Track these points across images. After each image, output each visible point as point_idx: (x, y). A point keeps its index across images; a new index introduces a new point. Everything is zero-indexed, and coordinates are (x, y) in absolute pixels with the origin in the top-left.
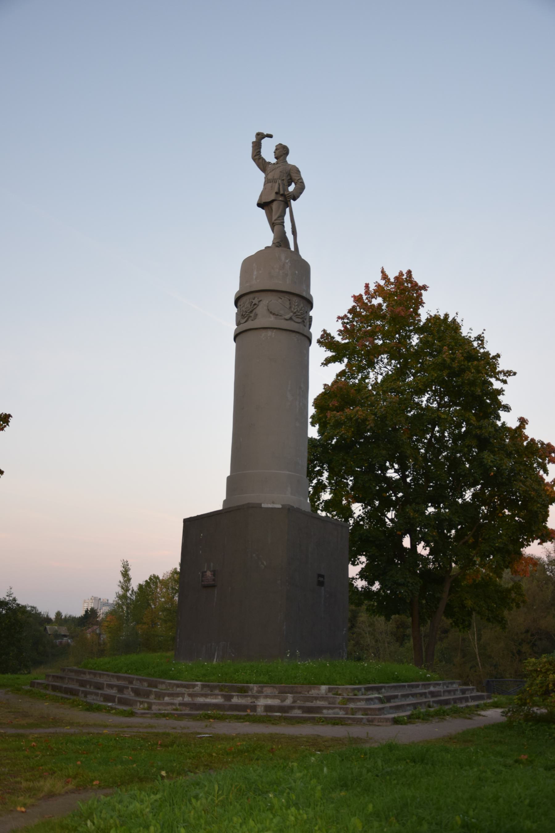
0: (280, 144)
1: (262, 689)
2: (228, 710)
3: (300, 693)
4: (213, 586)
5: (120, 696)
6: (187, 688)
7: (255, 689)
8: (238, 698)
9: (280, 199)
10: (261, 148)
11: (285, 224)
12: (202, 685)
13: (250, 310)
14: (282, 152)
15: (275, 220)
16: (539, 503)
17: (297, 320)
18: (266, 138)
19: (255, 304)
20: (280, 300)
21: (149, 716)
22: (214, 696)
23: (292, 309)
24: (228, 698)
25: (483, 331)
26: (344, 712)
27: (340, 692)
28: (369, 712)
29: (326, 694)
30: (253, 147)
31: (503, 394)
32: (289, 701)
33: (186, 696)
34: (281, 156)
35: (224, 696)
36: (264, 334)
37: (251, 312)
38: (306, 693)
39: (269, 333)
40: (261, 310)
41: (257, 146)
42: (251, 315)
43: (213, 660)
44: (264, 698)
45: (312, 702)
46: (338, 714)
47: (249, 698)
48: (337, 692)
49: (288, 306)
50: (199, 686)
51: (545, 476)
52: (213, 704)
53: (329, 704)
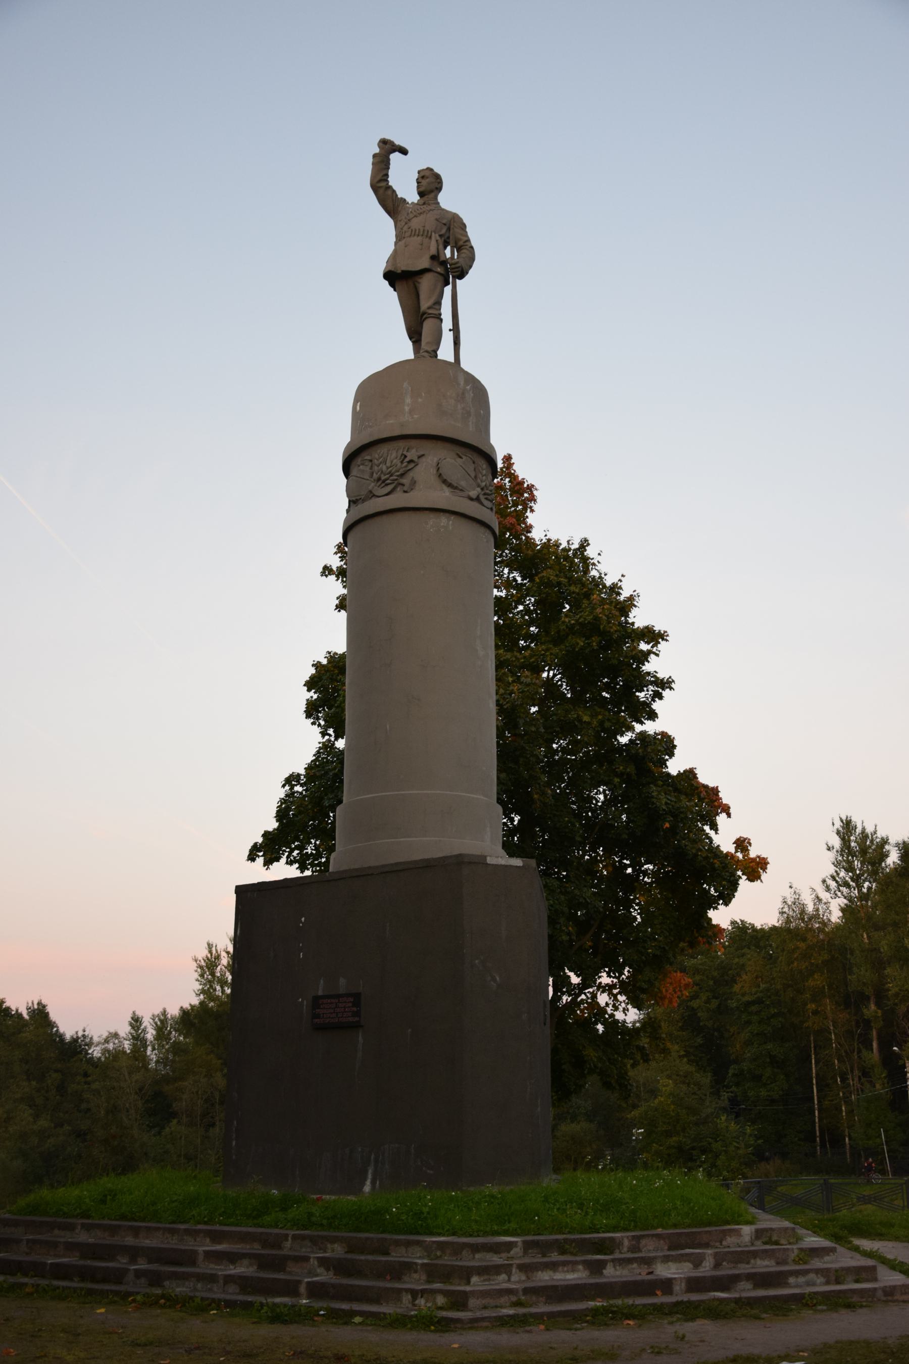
0: (430, 170)
3: (777, 1243)
4: (356, 1026)
5: (309, 1280)
7: (626, 1243)
8: (614, 1267)
9: (439, 270)
10: (389, 168)
12: (524, 1242)
13: (401, 471)
14: (430, 184)
15: (429, 308)
16: (725, 879)
18: (397, 153)
19: (411, 461)
20: (459, 460)
21: (485, 1324)
22: (570, 1267)
24: (596, 1268)
26: (822, 1280)
29: (752, 1244)
31: (671, 688)
32: (708, 1264)
33: (514, 1270)
34: (432, 191)
35: (589, 1265)
37: (402, 475)
38: (718, 1244)
39: (443, 520)
40: (424, 472)
41: (381, 164)
44: (662, 1262)
46: (814, 1284)
48: (770, 1238)
49: (473, 475)
50: (520, 1244)
51: (712, 833)
53: (778, 1263)
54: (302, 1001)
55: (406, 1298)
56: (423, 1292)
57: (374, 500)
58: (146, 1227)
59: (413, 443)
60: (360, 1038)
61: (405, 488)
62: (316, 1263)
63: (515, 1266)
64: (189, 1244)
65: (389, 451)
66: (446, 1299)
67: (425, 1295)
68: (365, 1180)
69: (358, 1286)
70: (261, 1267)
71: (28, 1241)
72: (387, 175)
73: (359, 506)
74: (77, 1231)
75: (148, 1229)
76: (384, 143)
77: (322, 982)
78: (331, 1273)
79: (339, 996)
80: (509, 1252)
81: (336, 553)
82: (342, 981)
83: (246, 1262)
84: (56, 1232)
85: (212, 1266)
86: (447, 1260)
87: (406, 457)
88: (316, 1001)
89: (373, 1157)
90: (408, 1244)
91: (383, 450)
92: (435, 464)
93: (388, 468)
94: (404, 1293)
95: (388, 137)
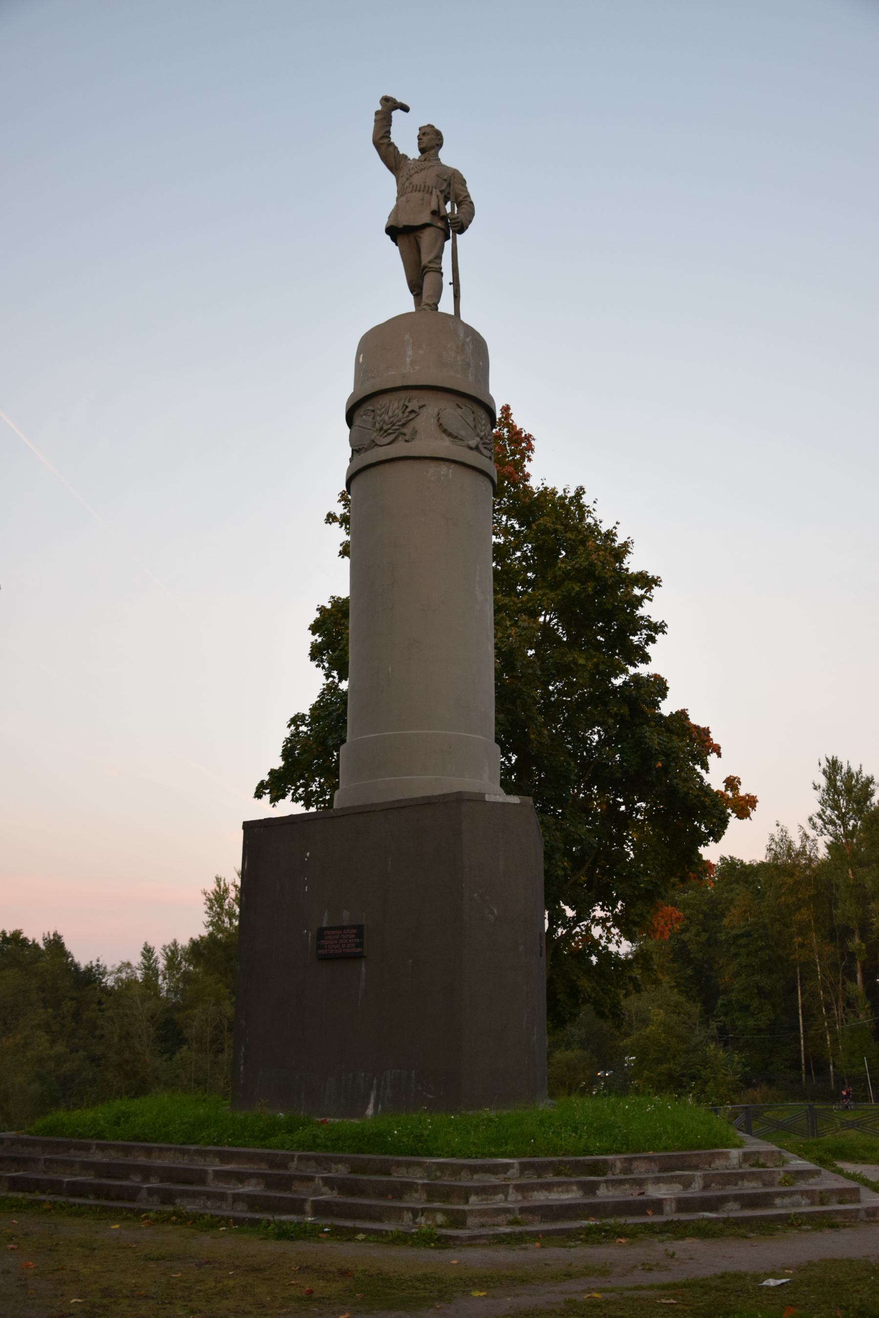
1: (631, 1165)
2: (611, 1216)
4: (359, 957)
5: (315, 1198)
6: (493, 1173)
7: (618, 1164)
8: (607, 1188)
9: (439, 225)
10: (390, 125)
11: (443, 271)
12: (520, 1164)
13: (403, 421)
14: (431, 139)
15: (430, 262)
16: (715, 817)
17: (485, 452)
19: (412, 411)
21: (483, 1241)
23: (478, 430)
24: (590, 1188)
25: (615, 524)
27: (762, 1161)
28: (847, 1197)
30: (375, 121)
31: (664, 632)
32: (697, 1185)
33: (511, 1191)
36: (432, 469)
38: (707, 1167)
40: (425, 422)
41: (383, 121)
42: (404, 430)
43: (365, 1108)
44: (653, 1183)
45: (736, 1185)
47: (627, 1186)
48: (758, 1160)
49: (472, 424)
50: (516, 1166)
51: (703, 773)
52: (561, 1206)
53: (764, 1185)
55: (407, 1217)
56: (423, 1210)
57: (376, 449)
58: (158, 1148)
60: (363, 968)
62: (321, 1182)
63: (511, 1186)
64: (199, 1164)
65: (390, 401)
67: (425, 1214)
68: (369, 1104)
70: (268, 1186)
71: (46, 1160)
72: (389, 132)
74: (92, 1151)
75: (160, 1149)
76: (386, 100)
77: (326, 914)
80: (506, 1173)
81: (340, 501)
82: (346, 914)
83: (253, 1181)
84: (72, 1151)
85: (221, 1185)
86: (447, 1180)
87: (407, 407)
88: (321, 933)
89: (375, 1082)
90: (409, 1165)
91: (384, 401)
92: (435, 415)
94: (405, 1212)
95: (389, 95)
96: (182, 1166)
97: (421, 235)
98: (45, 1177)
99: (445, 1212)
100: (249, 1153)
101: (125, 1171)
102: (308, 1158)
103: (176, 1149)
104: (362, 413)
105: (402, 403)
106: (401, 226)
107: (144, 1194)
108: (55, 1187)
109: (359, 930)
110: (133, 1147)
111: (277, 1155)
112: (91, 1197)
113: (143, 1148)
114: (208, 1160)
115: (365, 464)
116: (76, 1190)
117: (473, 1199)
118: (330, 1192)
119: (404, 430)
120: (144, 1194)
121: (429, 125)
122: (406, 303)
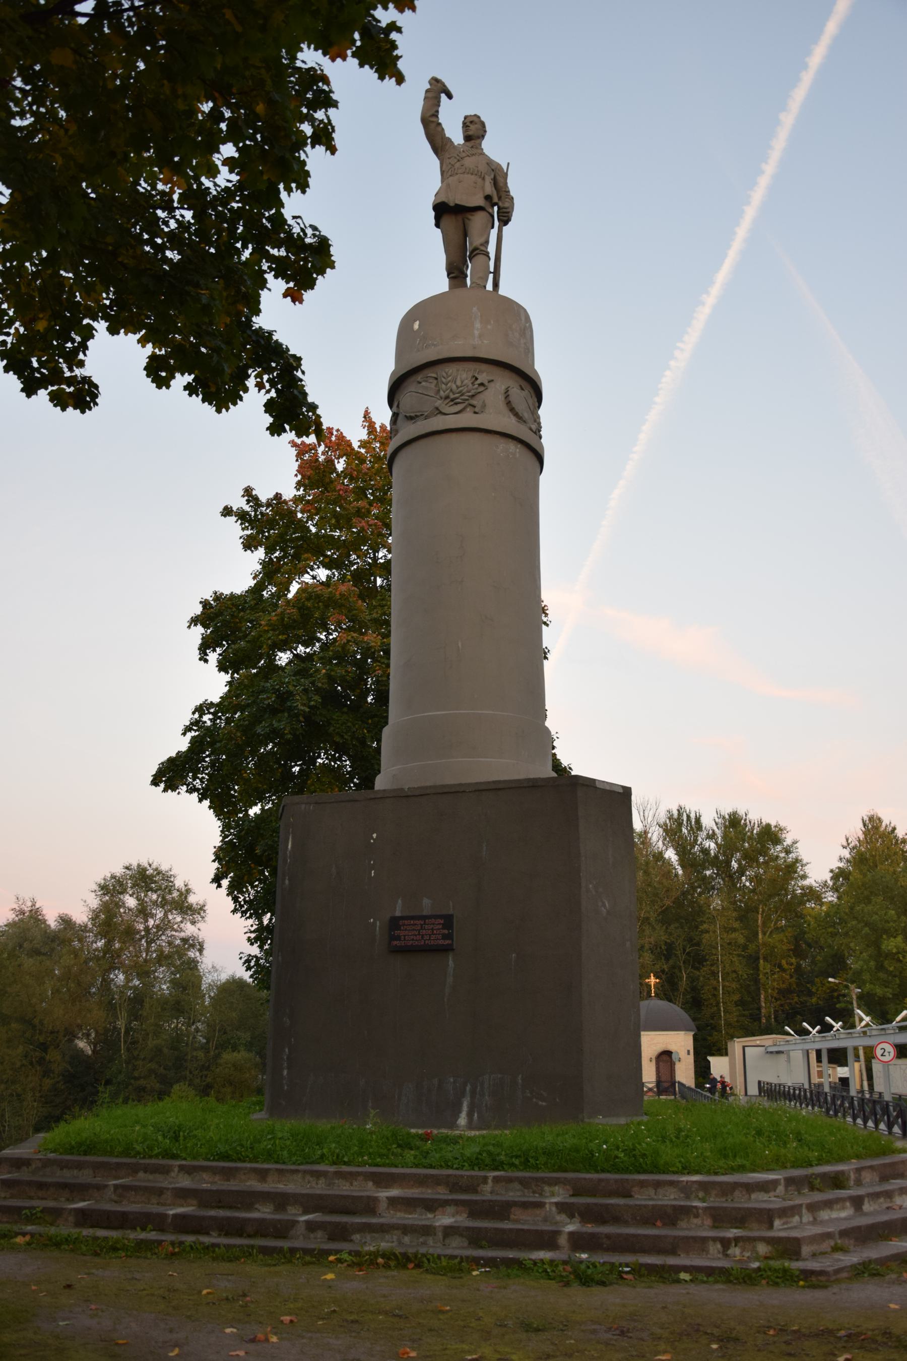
1: (860, 1175)
4: (447, 949)
10: (439, 106)
14: (474, 129)
19: (482, 384)
50: (782, 1181)
54: (374, 922)
55: (715, 1249)
56: (737, 1240)
57: (440, 417)
58: (277, 1170)
59: (484, 367)
60: (451, 962)
61: (476, 410)
62: (554, 1209)
63: (804, 1206)
64: (369, 1189)
65: (458, 370)
66: (770, 1248)
67: (740, 1244)
68: (460, 1112)
69: (645, 1236)
70: (472, 1215)
71: (116, 1187)
72: (438, 112)
73: (419, 423)
74: (173, 1174)
75: (280, 1172)
76: (435, 81)
77: (400, 901)
78: (577, 1219)
79: (424, 918)
80: (775, 1191)
81: (243, 496)
82: (426, 902)
83: (450, 1209)
84: (141, 1175)
85: (399, 1214)
86: (741, 1201)
87: (477, 379)
88: (394, 923)
89: (468, 1088)
90: (658, 1185)
91: (451, 369)
92: (503, 392)
93: (458, 387)
94: (711, 1243)
95: (439, 77)
96: (318, 1192)
97: (470, 217)
98: (118, 1208)
99: (769, 1241)
100: (419, 1175)
101: (249, 1199)
102: (510, 1180)
103: (305, 1172)
104: (419, 379)
105: (471, 374)
106: (452, 204)
107: (301, 1229)
108: (159, 1222)
109: (448, 921)
110: (237, 1169)
111: (462, 1176)
112: (213, 1234)
113: (255, 1170)
114: (355, 1183)
115: (423, 432)
116: (184, 1224)
117: (777, 1223)
118: (568, 1220)
119: (474, 402)
120: (301, 1229)
121: (475, 115)
122: (441, 284)
